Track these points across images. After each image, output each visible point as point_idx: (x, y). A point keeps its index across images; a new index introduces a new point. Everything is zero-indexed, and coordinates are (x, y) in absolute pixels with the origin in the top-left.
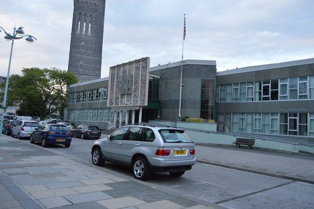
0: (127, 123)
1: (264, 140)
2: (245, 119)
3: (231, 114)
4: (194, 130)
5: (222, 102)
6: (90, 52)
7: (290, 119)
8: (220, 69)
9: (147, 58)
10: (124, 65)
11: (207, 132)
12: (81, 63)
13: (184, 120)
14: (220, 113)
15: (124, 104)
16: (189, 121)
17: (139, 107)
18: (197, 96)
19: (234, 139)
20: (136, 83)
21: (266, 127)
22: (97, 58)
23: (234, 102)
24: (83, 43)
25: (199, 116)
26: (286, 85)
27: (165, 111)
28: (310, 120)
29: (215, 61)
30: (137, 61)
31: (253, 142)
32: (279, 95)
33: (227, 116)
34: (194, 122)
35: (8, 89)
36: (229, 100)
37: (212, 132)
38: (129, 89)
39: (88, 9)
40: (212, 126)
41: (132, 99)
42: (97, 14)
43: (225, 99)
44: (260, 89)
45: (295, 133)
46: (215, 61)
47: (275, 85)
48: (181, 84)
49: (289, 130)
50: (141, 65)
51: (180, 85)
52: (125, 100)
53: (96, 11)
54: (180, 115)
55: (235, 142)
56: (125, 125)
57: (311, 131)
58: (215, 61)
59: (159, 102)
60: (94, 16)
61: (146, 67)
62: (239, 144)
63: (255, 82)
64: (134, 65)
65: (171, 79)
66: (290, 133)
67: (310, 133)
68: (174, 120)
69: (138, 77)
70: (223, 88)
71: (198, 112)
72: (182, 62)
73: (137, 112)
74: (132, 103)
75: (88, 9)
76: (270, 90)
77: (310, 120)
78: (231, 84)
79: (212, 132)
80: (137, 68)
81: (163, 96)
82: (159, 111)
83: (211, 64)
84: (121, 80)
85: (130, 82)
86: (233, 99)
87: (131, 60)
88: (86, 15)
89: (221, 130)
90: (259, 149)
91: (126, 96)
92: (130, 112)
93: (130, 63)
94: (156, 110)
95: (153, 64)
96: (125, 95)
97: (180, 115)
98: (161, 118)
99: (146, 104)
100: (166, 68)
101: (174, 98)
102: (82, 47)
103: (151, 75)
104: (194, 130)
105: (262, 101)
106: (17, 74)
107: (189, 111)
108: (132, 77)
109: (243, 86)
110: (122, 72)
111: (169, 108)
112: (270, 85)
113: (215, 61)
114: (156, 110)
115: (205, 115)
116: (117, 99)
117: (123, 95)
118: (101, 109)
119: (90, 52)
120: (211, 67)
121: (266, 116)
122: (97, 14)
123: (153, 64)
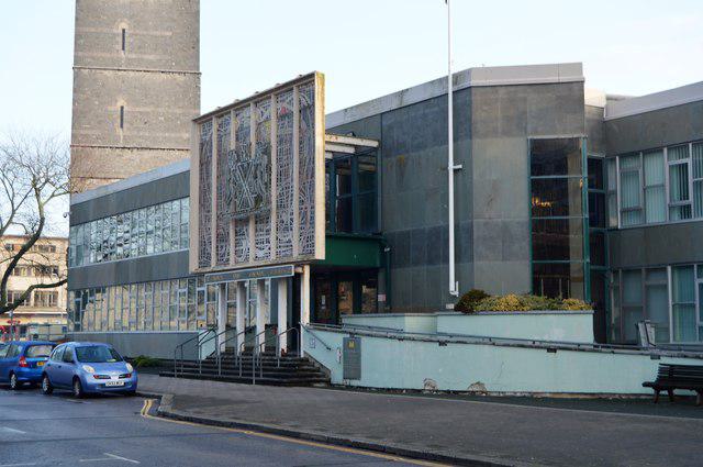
3: (665, 270)
4: (492, 342)
5: (634, 222)
6: (151, 57)
8: (594, 96)
9: (312, 75)
10: (239, 106)
11: (550, 350)
14: (627, 272)
15: (247, 259)
16: (492, 310)
17: (299, 264)
20: (284, 174)
22: (181, 78)
23: (676, 219)
24: (124, 25)
25: (528, 287)
27: (404, 276)
29: (578, 67)
30: (282, 90)
34: (519, 308)
35: (291, 145)
36: (657, 214)
37: (579, 348)
38: (258, 199)
40: (577, 325)
43: (639, 211)
46: (580, 65)
48: (451, 166)
50: (294, 101)
51: (446, 169)
52: (250, 242)
54: (453, 287)
55: (653, 378)
58: (578, 67)
59: (378, 241)
61: (311, 107)
63: (668, 150)
64: (273, 108)
65: (420, 147)
68: (432, 306)
69: (289, 152)
70: (631, 164)
71: (522, 270)
74: (273, 251)
78: (659, 150)
79: (579, 348)
80: (284, 116)
81: (395, 219)
82: (381, 276)
83: (564, 79)
84: (231, 165)
85: (259, 172)
86: (671, 208)
87: (262, 88)
89: (608, 336)
91: (251, 227)
93: (259, 99)
94: (374, 271)
95: (335, 100)
96: (246, 221)
97: (453, 287)
98: (388, 301)
99: (320, 253)
100: (394, 106)
101: (429, 223)
103: (333, 139)
104: (492, 342)
108: (267, 152)
110: (233, 136)
111: (416, 263)
113: (580, 65)
114: (374, 271)
115: (549, 285)
116: (222, 238)
117: (241, 223)
119: (151, 57)
120: (567, 91)
123: (335, 100)
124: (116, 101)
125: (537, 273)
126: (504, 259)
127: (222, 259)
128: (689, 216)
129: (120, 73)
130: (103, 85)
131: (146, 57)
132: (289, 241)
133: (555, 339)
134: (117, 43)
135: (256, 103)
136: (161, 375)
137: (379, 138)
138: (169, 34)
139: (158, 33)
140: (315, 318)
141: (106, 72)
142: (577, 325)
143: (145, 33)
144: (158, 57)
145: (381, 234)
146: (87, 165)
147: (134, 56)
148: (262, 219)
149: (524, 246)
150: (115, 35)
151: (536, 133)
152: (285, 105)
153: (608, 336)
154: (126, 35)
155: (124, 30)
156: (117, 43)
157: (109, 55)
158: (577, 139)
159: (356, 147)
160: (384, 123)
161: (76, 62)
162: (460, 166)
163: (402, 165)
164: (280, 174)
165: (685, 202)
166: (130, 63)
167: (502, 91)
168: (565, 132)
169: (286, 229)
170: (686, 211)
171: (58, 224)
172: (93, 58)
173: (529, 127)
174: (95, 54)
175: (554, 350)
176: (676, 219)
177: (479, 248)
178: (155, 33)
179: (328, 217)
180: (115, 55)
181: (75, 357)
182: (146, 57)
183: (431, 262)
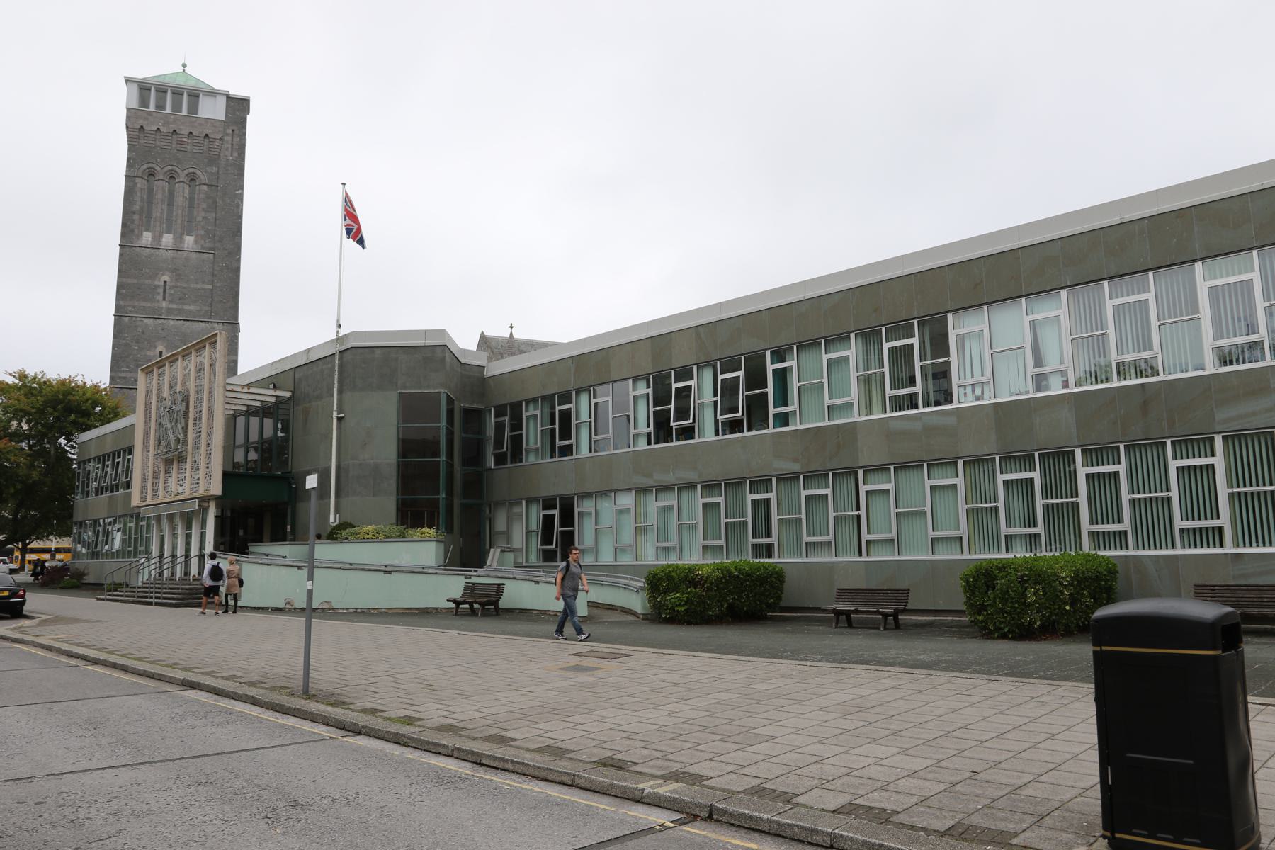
1: (537, 582)
2: (589, 513)
4: (352, 567)
6: (192, 308)
7: (753, 501)
11: (386, 572)
12: (160, 348)
24: (166, 278)
25: (394, 520)
26: (847, 359)
28: (867, 492)
29: (442, 332)
34: (374, 537)
37: (422, 571)
39: (180, 155)
41: (188, 475)
47: (756, 379)
48: (335, 415)
49: (1179, 523)
53: (213, 160)
54: (332, 519)
57: (872, 537)
60: (202, 177)
62: (848, 613)
71: (389, 504)
72: (340, 340)
75: (180, 155)
77: (867, 492)
79: (422, 571)
83: (429, 343)
88: (172, 176)
90: (512, 613)
91: (175, 466)
102: (161, 290)
104: (352, 567)
105: (653, 446)
106: (64, 376)
109: (808, 356)
116: (156, 476)
117: (168, 462)
119: (192, 308)
121: (908, 478)
122: (215, 170)
124: (156, 347)
126: (374, 495)
127: (155, 495)
129: (160, 321)
130: (143, 333)
131: (186, 307)
132: (199, 479)
133: (403, 563)
134: (158, 294)
135: (184, 356)
136: (98, 599)
137: (292, 389)
138: (210, 287)
139: (198, 286)
141: (146, 320)
143: (185, 285)
144: (198, 308)
145: (289, 473)
146: (489, 350)
147: (174, 306)
148: (182, 459)
149: (391, 484)
150: (159, 286)
151: (405, 388)
154: (168, 287)
155: (165, 282)
156: (158, 294)
157: (149, 305)
158: (440, 393)
159: (277, 397)
160: (296, 375)
161: (117, 310)
162: (343, 415)
163: (306, 412)
164: (195, 419)
166: (169, 310)
167: (378, 352)
168: (428, 387)
169: (157, 478)
172: (134, 307)
174: (136, 304)
175: (390, 572)
178: (195, 286)
179: (332, 439)
180: (156, 305)
181: (1040, 370)
182: (186, 307)
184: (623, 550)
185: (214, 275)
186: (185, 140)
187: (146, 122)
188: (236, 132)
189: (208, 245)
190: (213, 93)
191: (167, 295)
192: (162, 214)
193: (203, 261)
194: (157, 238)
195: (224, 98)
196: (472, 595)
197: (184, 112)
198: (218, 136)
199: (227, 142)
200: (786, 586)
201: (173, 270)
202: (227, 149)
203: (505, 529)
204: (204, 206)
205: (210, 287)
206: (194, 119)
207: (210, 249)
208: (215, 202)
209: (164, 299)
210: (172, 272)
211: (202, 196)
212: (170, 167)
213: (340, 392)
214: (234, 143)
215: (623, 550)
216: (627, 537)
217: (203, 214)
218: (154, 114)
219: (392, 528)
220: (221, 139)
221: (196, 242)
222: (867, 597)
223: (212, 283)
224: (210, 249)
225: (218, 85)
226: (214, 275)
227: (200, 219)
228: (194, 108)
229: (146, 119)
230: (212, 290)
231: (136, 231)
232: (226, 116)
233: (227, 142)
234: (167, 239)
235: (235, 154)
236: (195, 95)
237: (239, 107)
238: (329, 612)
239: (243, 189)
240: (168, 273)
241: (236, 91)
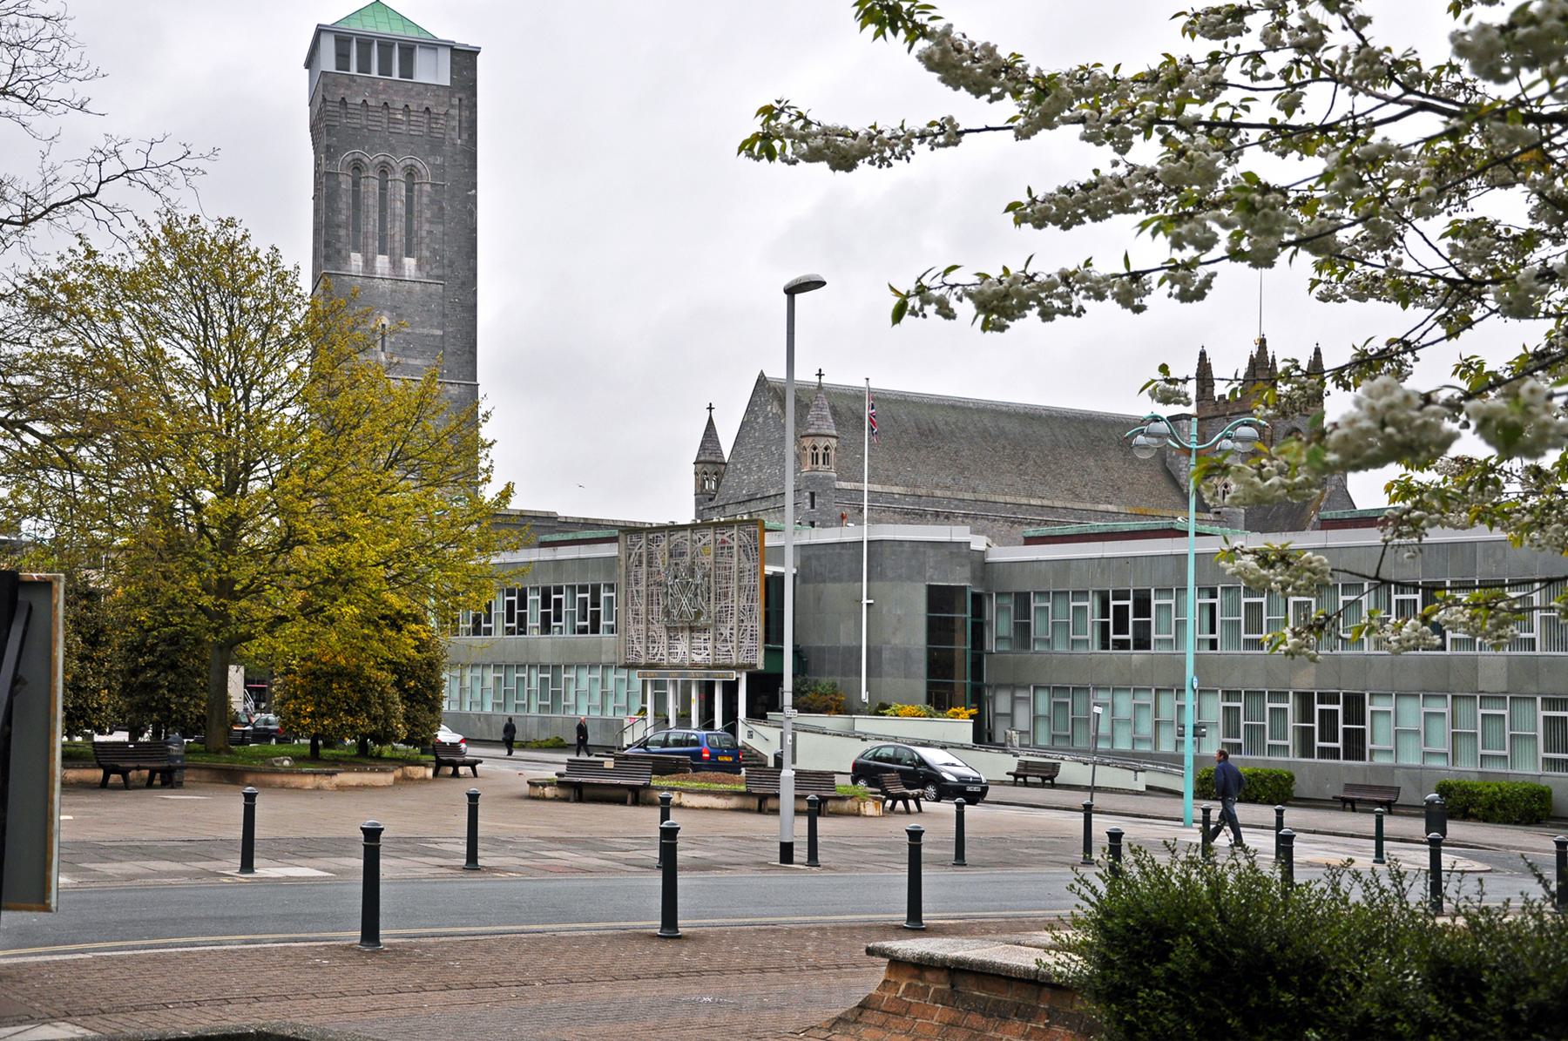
0: (534, 597)
6: (418, 362)
13: (880, 709)
18: (916, 637)
19: (1012, 764)
21: (1464, 746)
28: (1372, 712)
31: (1055, 768)
32: (1154, 636)
33: (1019, 694)
40: (961, 728)
42: (439, 160)
44: (1105, 614)
45: (1334, 753)
48: (865, 601)
54: (864, 696)
56: (792, 863)
66: (1324, 753)
67: (1372, 751)
71: (920, 686)
73: (730, 689)
76: (1131, 619)
77: (1372, 712)
88: (384, 169)
89: (983, 737)
92: (707, 689)
97: (864, 696)
101: (844, 641)
107: (891, 685)
109: (1060, 603)
112: (1130, 603)
118: (497, 667)
119: (418, 362)
122: (439, 160)
125: (930, 686)
128: (1215, 648)
131: (411, 362)
138: (439, 332)
139: (425, 331)
140: (748, 715)
142: (961, 728)
144: (427, 363)
149: (922, 668)
151: (933, 580)
152: (725, 537)
153: (983, 737)
165: (1213, 636)
168: (955, 580)
170: (1213, 644)
171: (343, 600)
173: (928, 575)
176: (1206, 650)
177: (886, 667)
182: (411, 362)
183: (844, 674)
184: (1141, 740)
185: (445, 316)
186: (399, 117)
187: (349, 92)
188: (465, 102)
189: (436, 272)
190: (434, 45)
191: (387, 344)
192: (374, 226)
193: (430, 296)
194: (369, 263)
195: (448, 52)
196: (1025, 770)
197: (396, 76)
198: (442, 110)
199: (454, 118)
200: (1554, 795)
201: (394, 309)
202: (454, 129)
203: (1009, 711)
204: (428, 214)
205: (439, 332)
206: (410, 86)
207: (438, 277)
208: (442, 209)
209: (383, 350)
210: (392, 311)
211: (425, 200)
212: (382, 158)
213: (868, 580)
214: (463, 119)
215: (1141, 740)
216: (1146, 728)
217: (426, 227)
218: (358, 80)
219: (922, 706)
220: (445, 114)
221: (419, 267)
222: (881, 858)
223: (442, 326)
224: (438, 277)
225: (442, 33)
226: (445, 316)
227: (424, 234)
228: (407, 70)
229: (348, 87)
230: (442, 337)
231: (343, 252)
232: (452, 78)
233: (454, 118)
234: (382, 263)
235: (465, 136)
236: (408, 50)
237: (465, 59)
238: (1087, 788)
239: (476, 189)
240: (386, 312)
241: (463, 38)
